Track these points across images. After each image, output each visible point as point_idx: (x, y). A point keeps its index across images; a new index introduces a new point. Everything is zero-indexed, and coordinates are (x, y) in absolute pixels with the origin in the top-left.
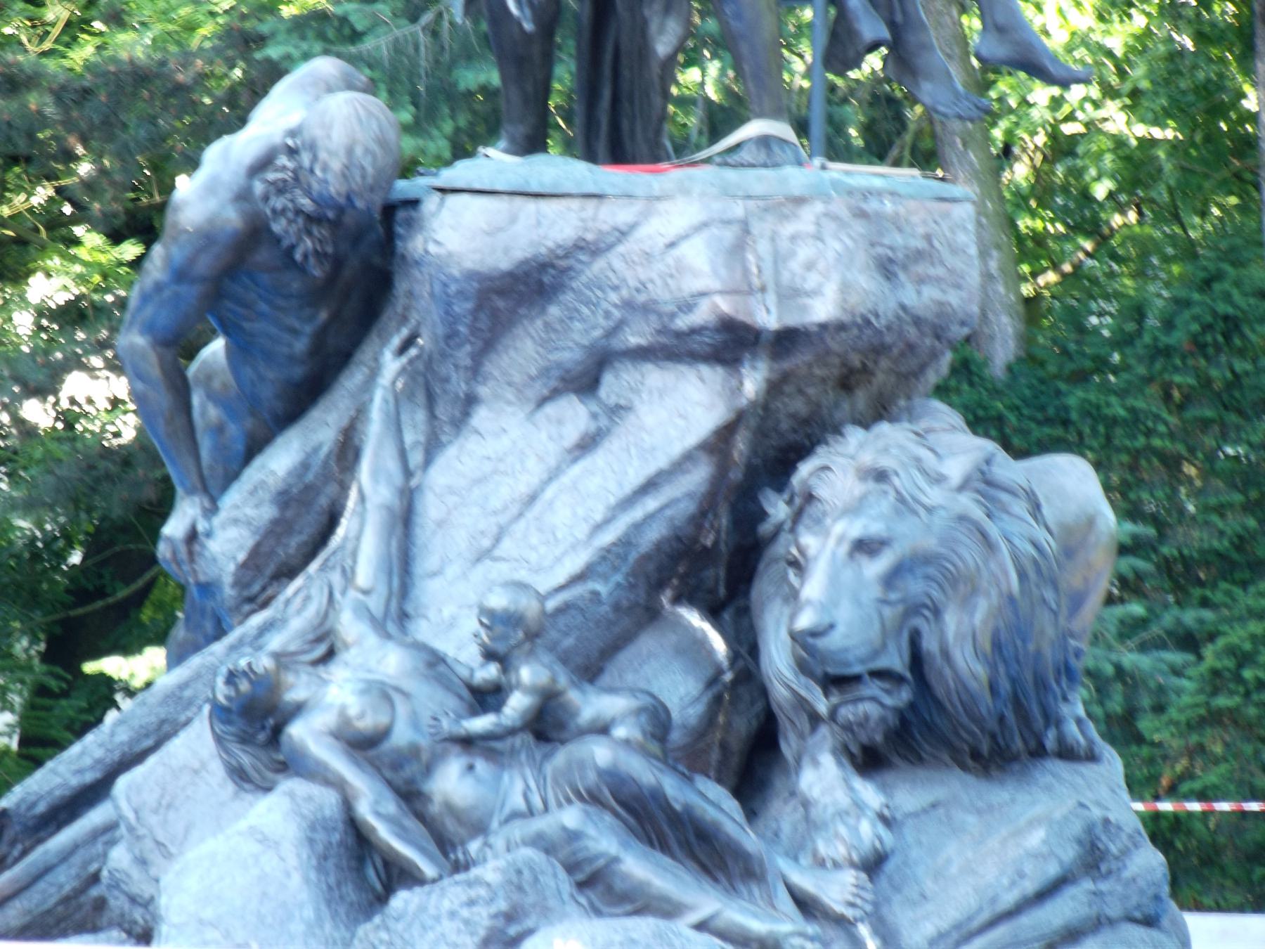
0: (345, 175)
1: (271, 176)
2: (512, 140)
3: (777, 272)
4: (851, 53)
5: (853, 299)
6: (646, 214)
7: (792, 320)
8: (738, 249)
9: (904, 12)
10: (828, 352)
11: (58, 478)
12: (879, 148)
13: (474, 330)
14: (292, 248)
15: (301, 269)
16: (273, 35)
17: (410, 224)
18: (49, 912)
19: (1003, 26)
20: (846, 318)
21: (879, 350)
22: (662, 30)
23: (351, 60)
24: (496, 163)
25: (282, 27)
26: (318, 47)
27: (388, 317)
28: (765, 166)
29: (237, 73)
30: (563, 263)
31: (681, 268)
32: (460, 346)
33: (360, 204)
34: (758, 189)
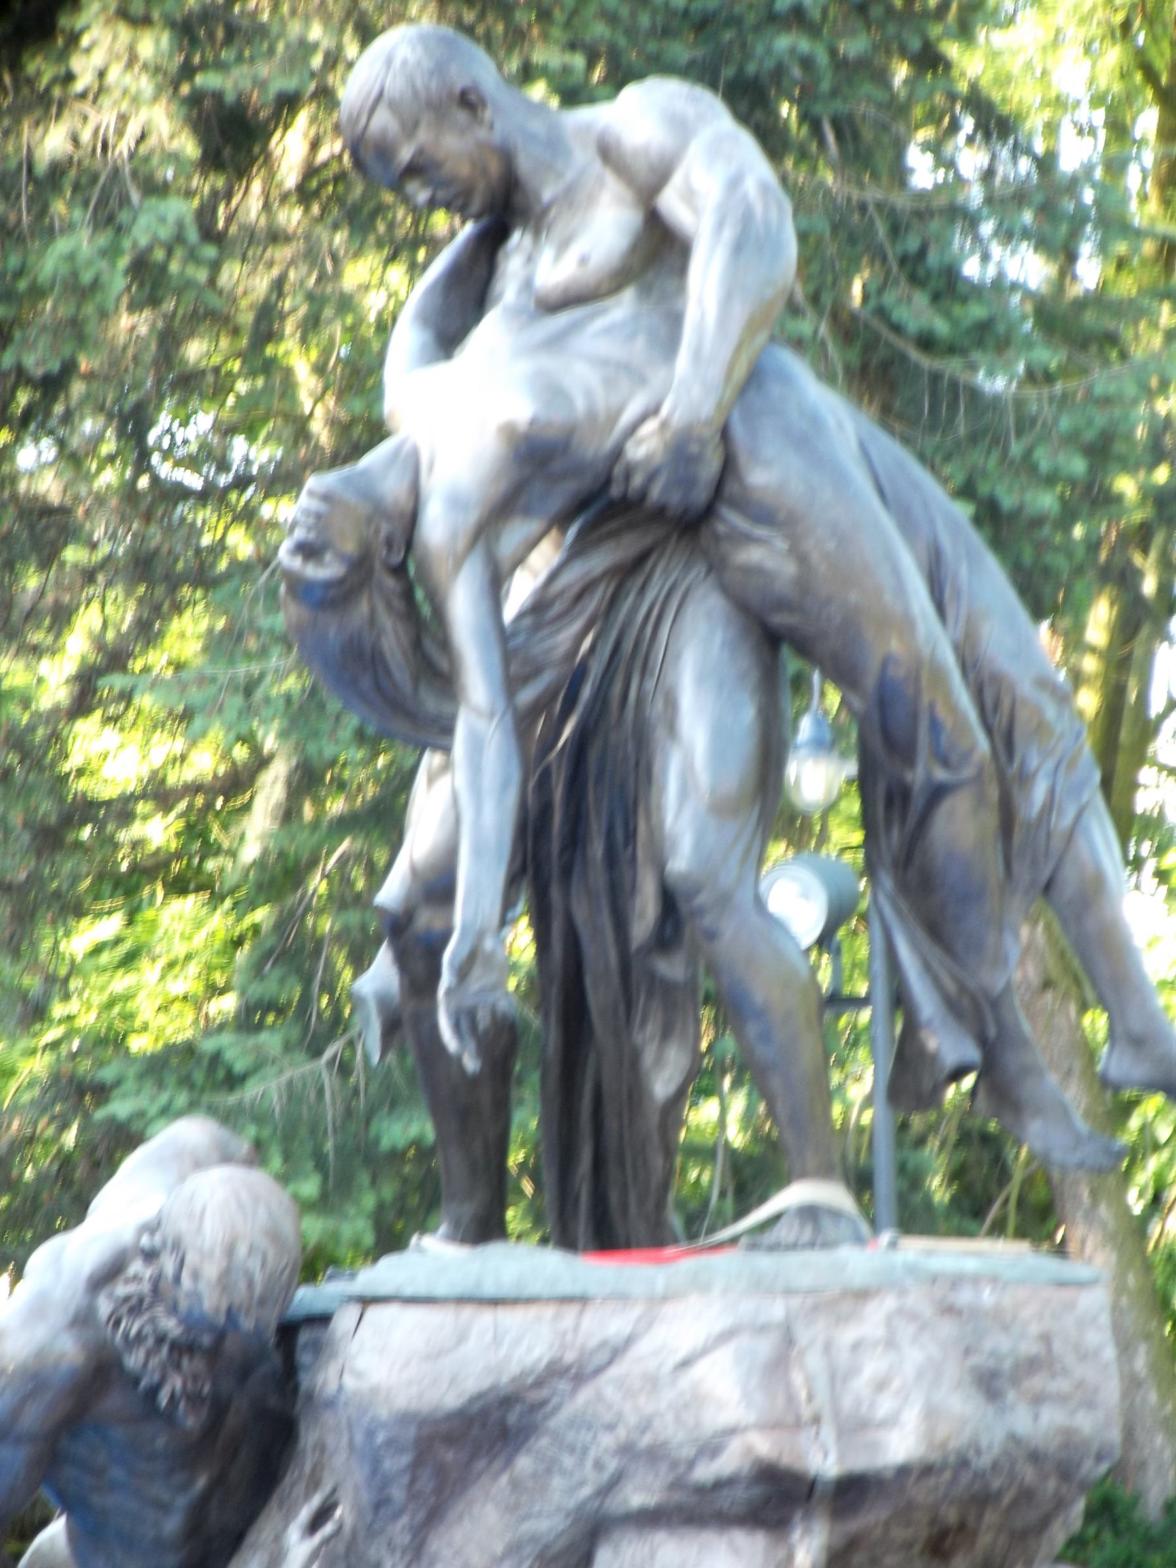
0: (225, 1280)
1: (122, 1289)
2: (456, 1225)
3: (835, 1398)
4: (927, 1084)
5: (943, 1430)
6: (647, 1322)
7: (859, 1463)
8: (780, 1363)
9: (999, 1022)
10: (910, 1506)
12: (972, 1210)
13: (413, 1494)
14: (154, 1391)
15: (169, 1417)
16: (118, 1083)
17: (317, 1348)
19: (1169, 604)
20: (934, 1457)
21: (982, 1499)
22: (659, 1059)
23: (229, 1118)
24: (435, 1256)
25: (132, 1072)
26: (182, 1099)
27: (293, 1479)
28: (812, 1245)
29: (70, 1138)
30: (534, 1396)
31: (696, 1400)
32: (396, 1516)
33: (247, 1324)
34: (805, 1280)
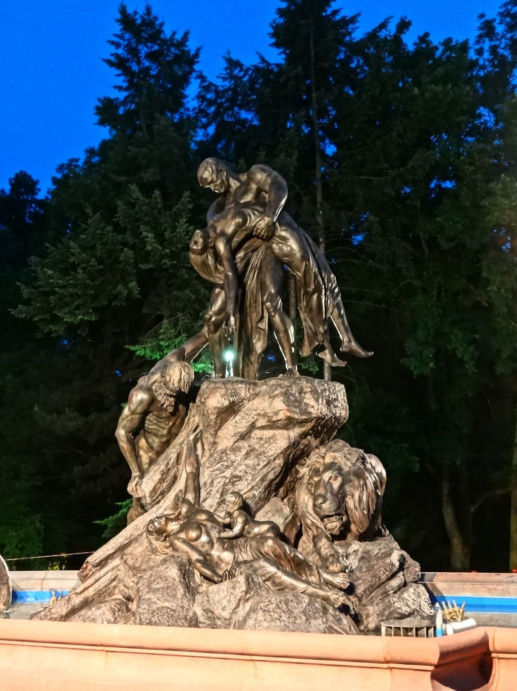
11: (237, 510)
18: (101, 590)
